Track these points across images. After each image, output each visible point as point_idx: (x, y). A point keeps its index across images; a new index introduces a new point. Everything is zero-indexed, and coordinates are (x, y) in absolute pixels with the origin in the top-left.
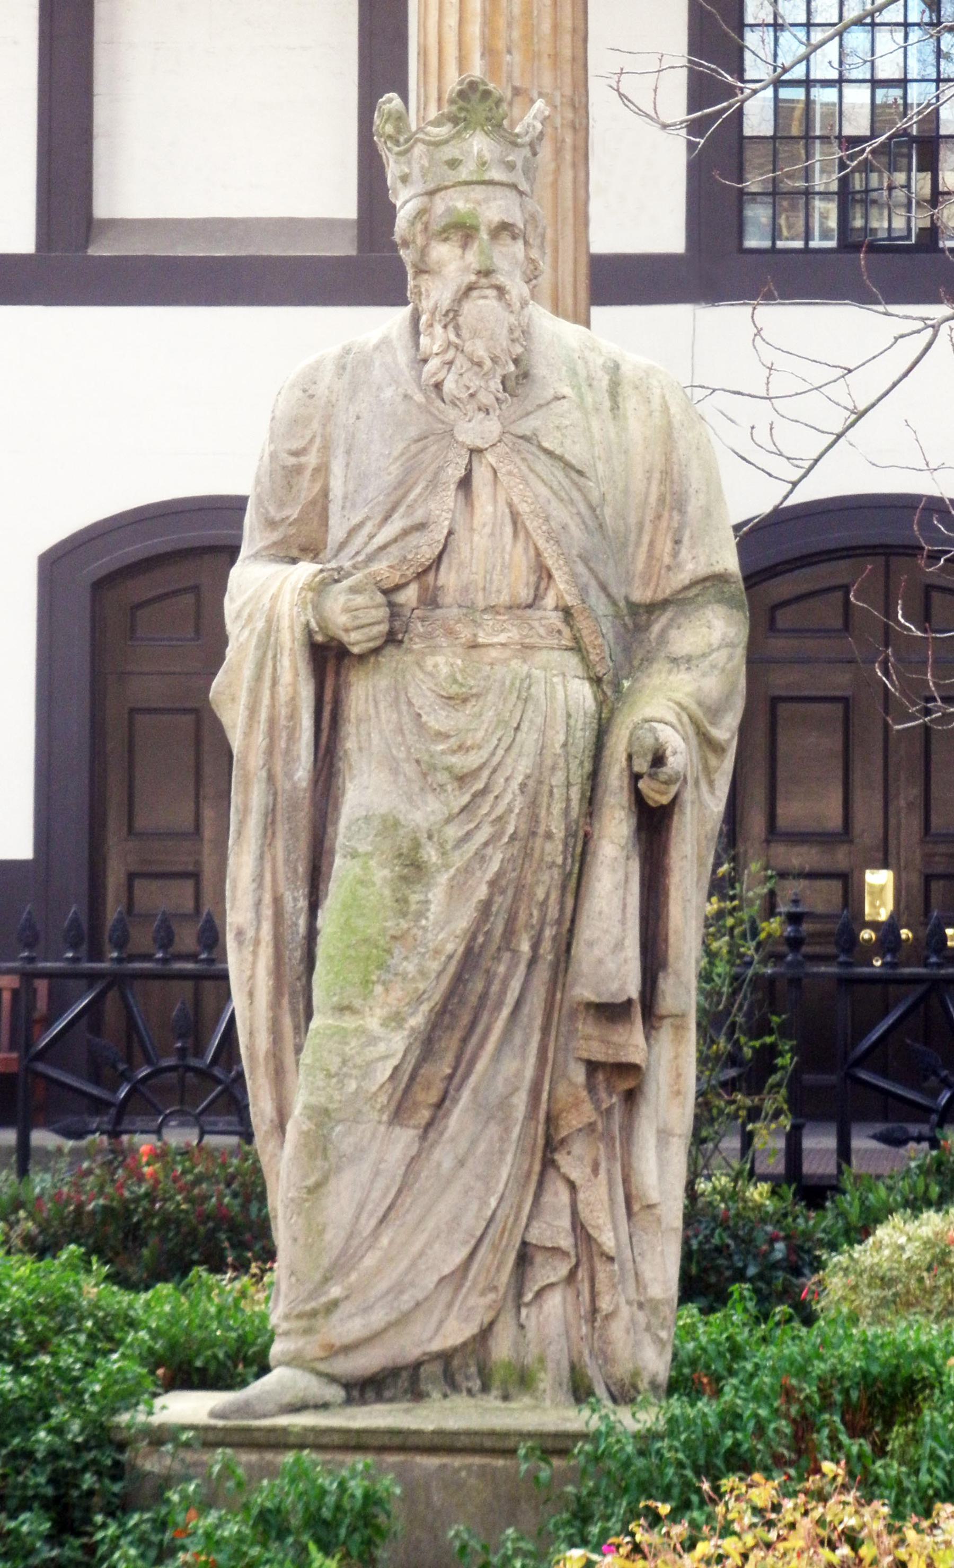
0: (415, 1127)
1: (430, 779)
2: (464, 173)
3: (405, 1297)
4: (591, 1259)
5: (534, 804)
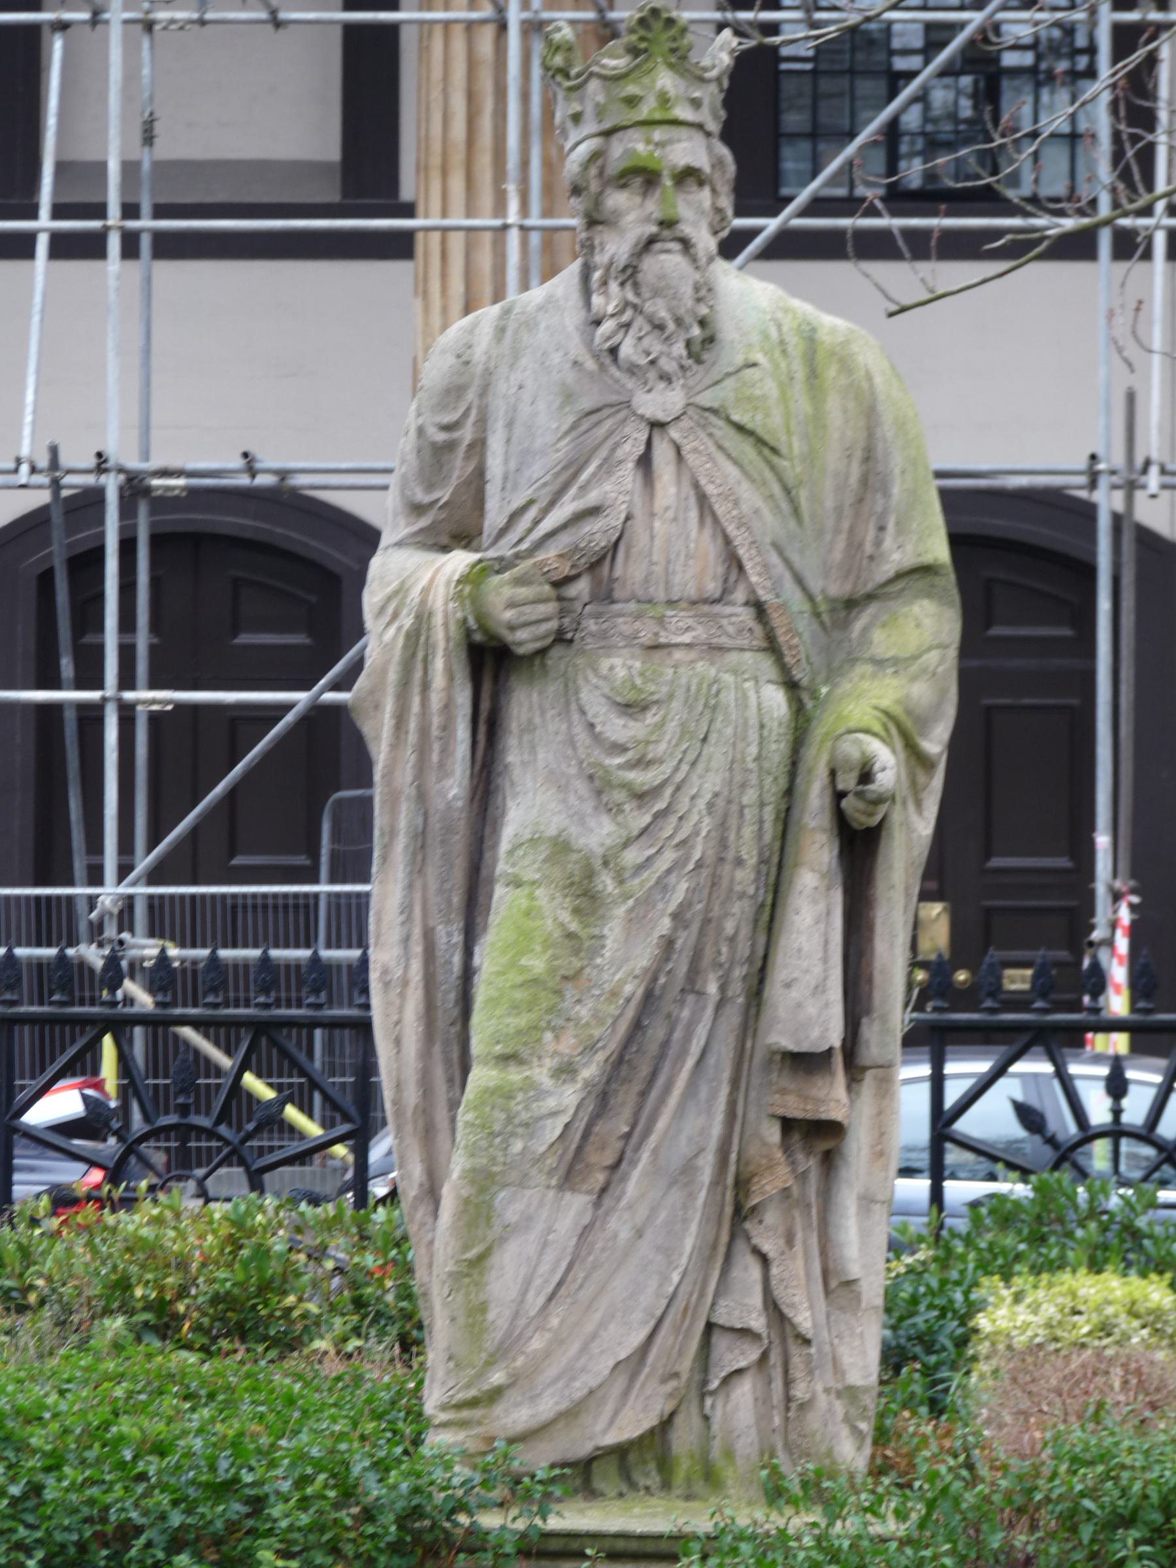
0: (589, 1192)
1: (605, 800)
2: (645, 111)
3: (577, 1384)
4: (784, 1340)
5: (722, 825)
